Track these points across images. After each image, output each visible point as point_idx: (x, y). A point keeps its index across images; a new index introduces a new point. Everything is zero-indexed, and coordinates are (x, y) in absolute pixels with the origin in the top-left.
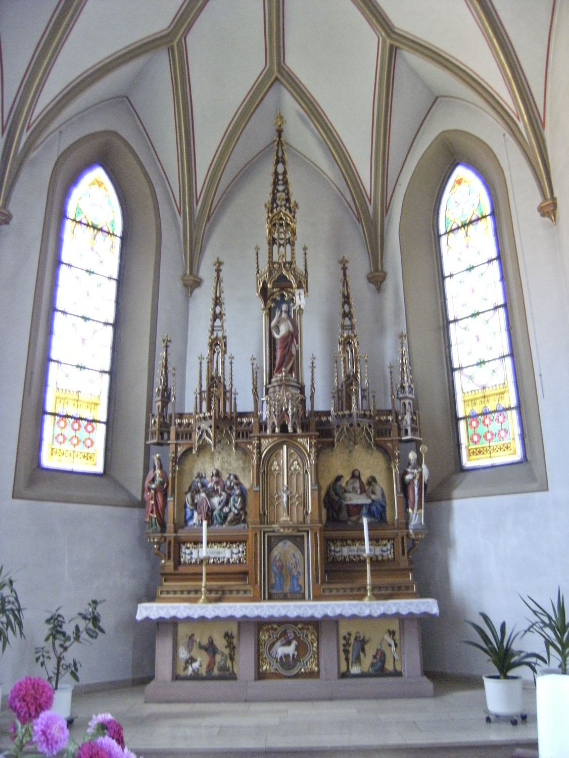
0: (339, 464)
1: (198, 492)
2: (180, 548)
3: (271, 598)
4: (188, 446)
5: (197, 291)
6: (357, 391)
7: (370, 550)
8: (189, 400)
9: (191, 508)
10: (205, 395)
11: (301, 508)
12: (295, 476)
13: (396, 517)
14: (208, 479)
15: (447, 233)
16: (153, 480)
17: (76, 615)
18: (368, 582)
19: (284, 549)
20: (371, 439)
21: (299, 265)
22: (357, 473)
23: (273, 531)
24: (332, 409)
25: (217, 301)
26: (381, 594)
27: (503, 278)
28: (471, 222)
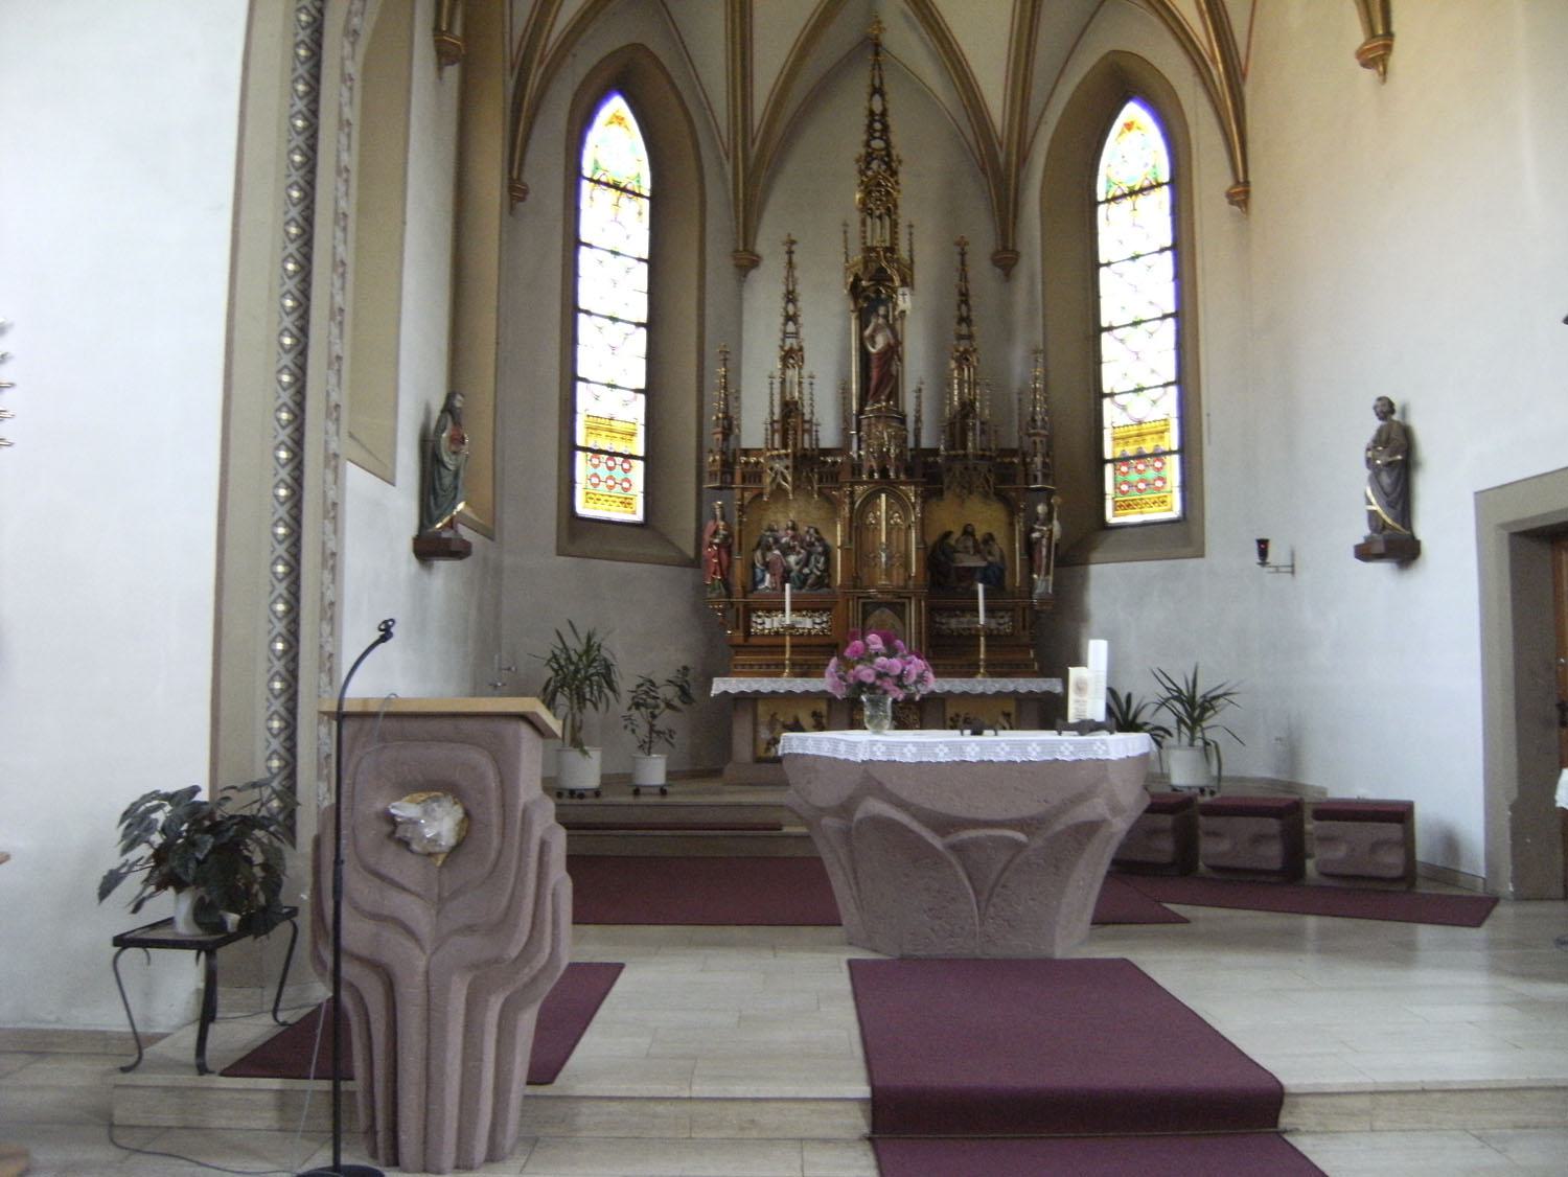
0: (950, 516)
1: (769, 548)
4: (756, 492)
5: (753, 274)
6: (974, 425)
8: (754, 430)
9: (762, 568)
11: (902, 571)
12: (895, 529)
13: (1017, 584)
14: (782, 533)
15: (1108, 201)
16: (715, 533)
18: (982, 656)
20: (989, 486)
21: (903, 253)
22: (970, 529)
23: (869, 597)
24: (942, 447)
25: (790, 297)
26: (995, 671)
27: (1178, 277)
28: (1142, 190)
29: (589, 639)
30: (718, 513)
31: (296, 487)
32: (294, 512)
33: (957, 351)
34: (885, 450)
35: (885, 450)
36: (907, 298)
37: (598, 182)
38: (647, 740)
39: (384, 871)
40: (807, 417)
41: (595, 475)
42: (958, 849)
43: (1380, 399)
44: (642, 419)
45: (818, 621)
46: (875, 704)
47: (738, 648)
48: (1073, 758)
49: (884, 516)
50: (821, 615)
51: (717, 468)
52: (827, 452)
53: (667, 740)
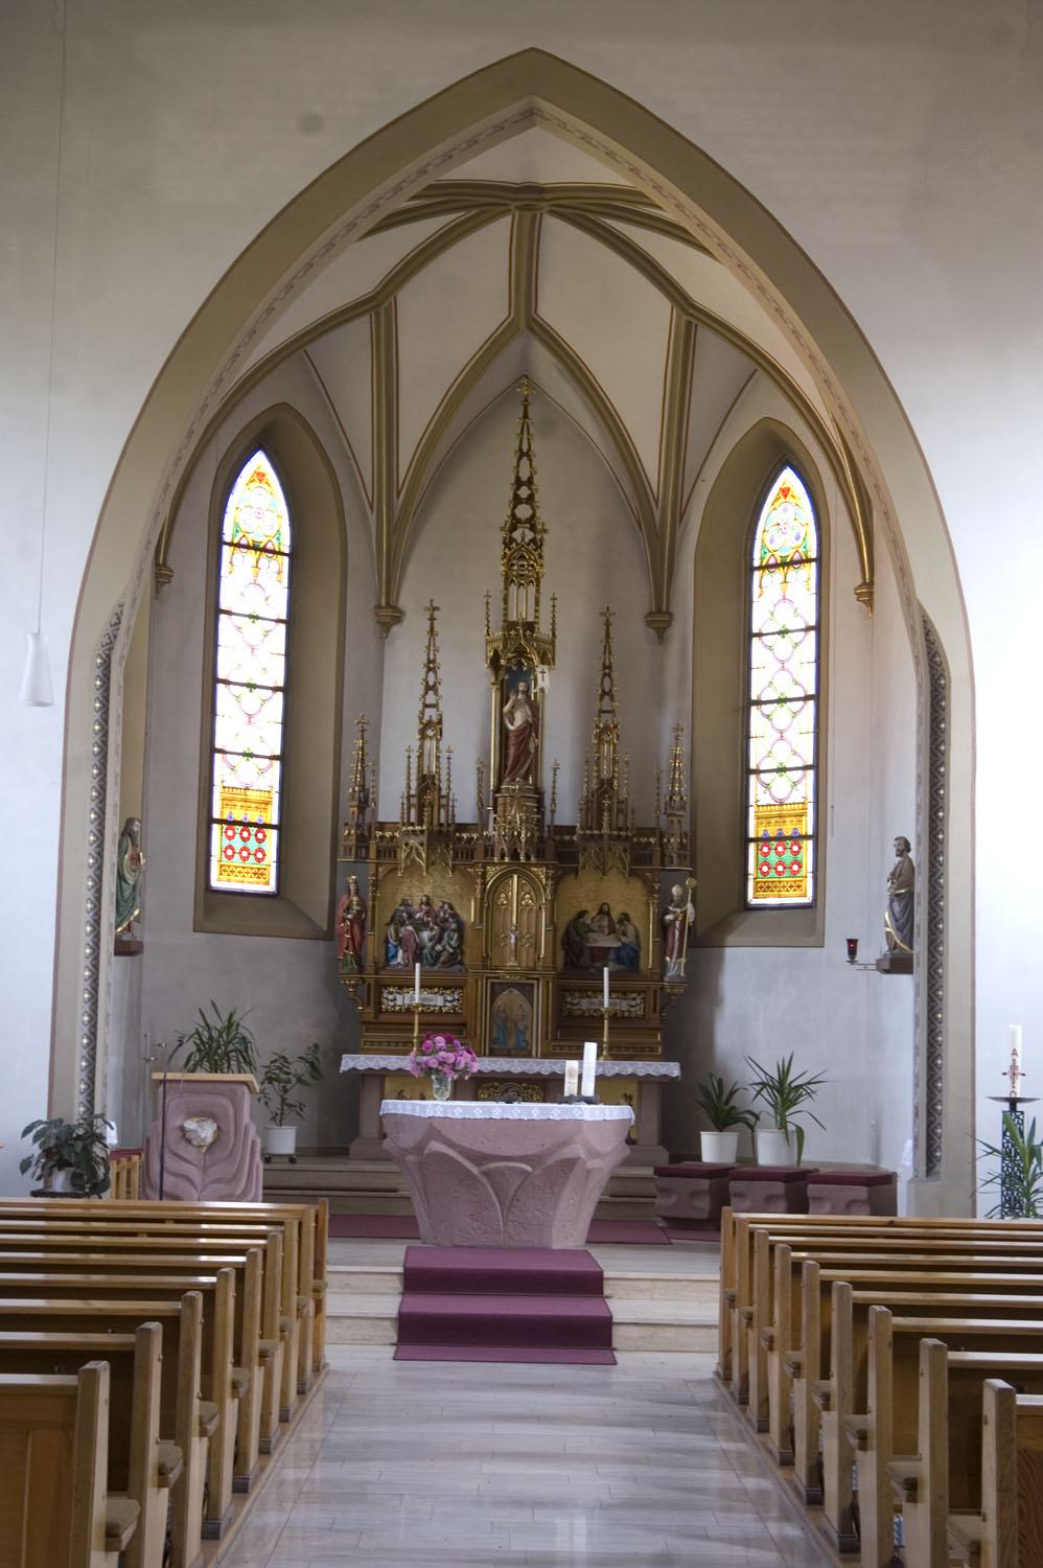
1: (403, 924)
2: (381, 993)
3: (492, 1054)
4: (390, 866)
5: (395, 629)
7: (610, 1004)
8: (390, 806)
9: (395, 943)
10: (414, 801)
11: (532, 950)
12: (525, 912)
14: (416, 907)
16: (348, 909)
17: (296, 1059)
18: (605, 1040)
19: (511, 999)
21: (544, 629)
22: (605, 908)
23: (497, 978)
24: (578, 825)
25: (431, 666)
28: (793, 563)
29: (231, 1016)
30: (352, 888)
31: (96, 948)
32: (94, 962)
33: (597, 727)
34: (516, 833)
35: (516, 833)
36: (546, 675)
37: (239, 545)
38: (279, 1112)
39: (179, 1153)
40: (444, 793)
41: (230, 847)
42: (486, 1174)
43: (897, 839)
44: (276, 787)
45: (449, 998)
46: (441, 1081)
47: (368, 1025)
48: (560, 1118)
49: (515, 896)
50: (453, 993)
51: (353, 842)
52: (463, 827)
53: (298, 1114)
